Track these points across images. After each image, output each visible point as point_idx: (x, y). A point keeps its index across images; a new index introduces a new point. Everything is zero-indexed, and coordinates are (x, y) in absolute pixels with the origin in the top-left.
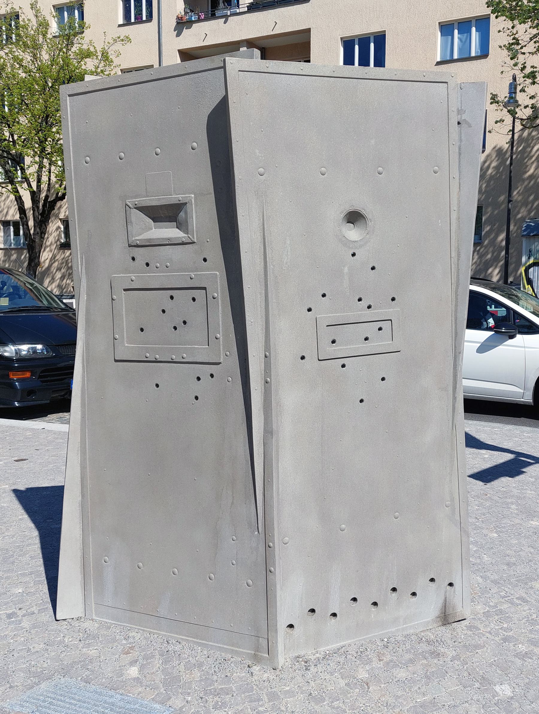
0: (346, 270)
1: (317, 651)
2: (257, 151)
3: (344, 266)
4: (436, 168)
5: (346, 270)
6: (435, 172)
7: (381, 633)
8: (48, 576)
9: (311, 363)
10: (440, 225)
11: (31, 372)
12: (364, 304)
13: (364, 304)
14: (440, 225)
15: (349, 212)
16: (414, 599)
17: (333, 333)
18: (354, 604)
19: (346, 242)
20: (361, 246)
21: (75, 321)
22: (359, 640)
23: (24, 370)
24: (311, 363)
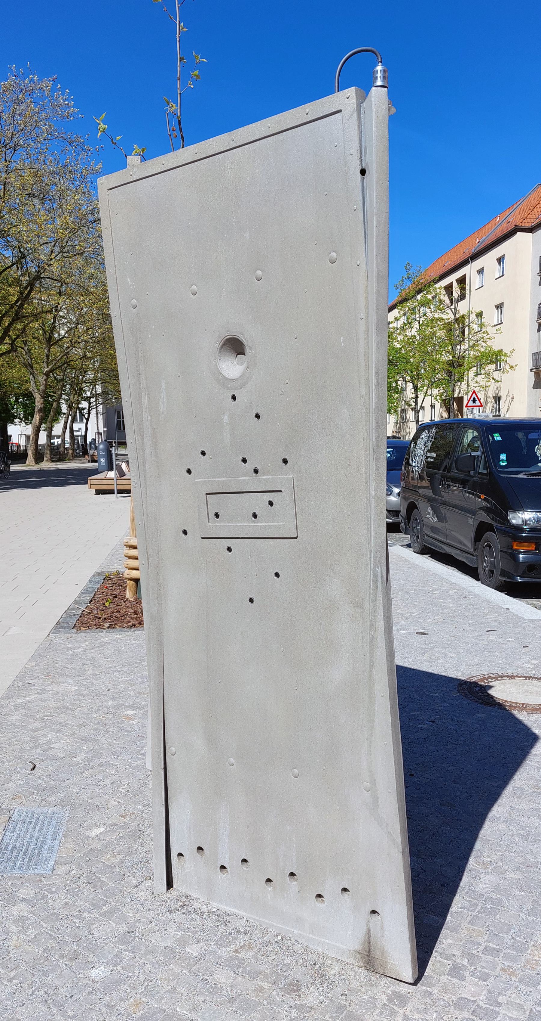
0: (226, 418)
1: (210, 903)
2: (129, 280)
3: (224, 414)
4: (334, 254)
5: (226, 418)
6: (333, 262)
7: (281, 926)
8: (415, 865)
9: (193, 540)
10: (343, 344)
11: (536, 545)
12: (250, 466)
13: (250, 466)
14: (343, 344)
15: (227, 340)
16: (318, 904)
17: (215, 502)
18: (244, 867)
19: (224, 381)
20: (243, 385)
21: (476, 457)
22: (255, 920)
23: (531, 541)
24: (193, 540)
